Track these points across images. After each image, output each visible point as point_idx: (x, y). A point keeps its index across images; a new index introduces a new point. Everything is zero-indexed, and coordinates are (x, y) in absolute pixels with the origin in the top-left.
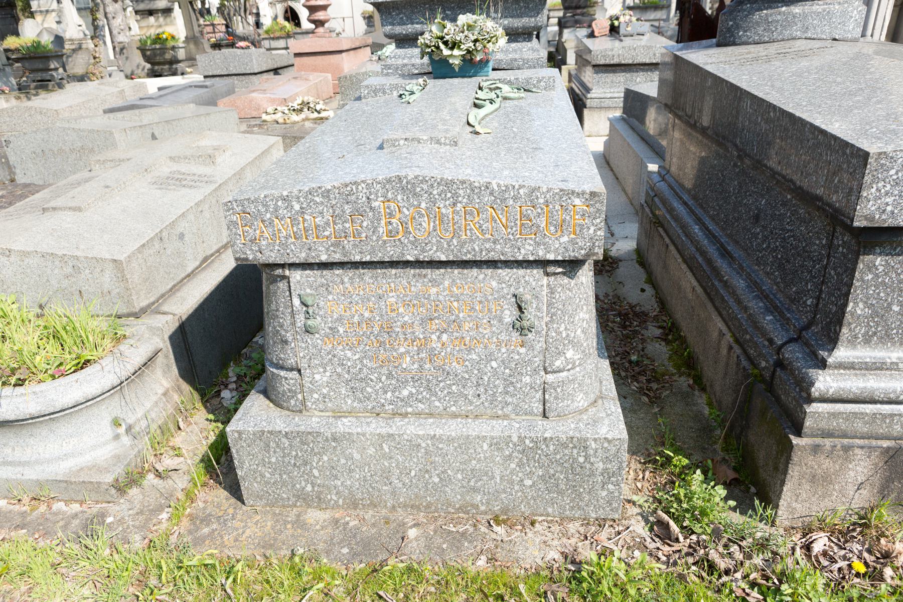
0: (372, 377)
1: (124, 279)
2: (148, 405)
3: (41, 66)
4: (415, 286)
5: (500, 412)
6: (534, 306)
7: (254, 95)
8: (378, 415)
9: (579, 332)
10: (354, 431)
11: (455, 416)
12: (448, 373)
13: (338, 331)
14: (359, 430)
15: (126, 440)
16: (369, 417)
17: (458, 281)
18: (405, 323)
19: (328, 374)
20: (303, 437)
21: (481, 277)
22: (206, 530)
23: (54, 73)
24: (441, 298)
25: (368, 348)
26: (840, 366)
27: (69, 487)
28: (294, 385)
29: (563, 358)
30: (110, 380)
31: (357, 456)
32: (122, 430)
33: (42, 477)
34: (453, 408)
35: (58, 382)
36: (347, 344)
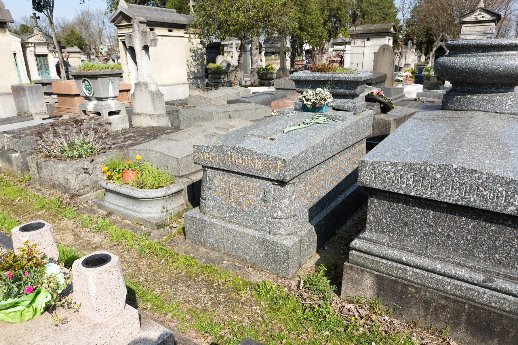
1: (178, 165)
2: (175, 206)
3: (218, 77)
7: (287, 101)
9: (284, 206)
10: (215, 223)
11: (244, 226)
15: (165, 214)
20: (203, 221)
22: (173, 244)
23: (222, 80)
26: (364, 238)
27: (145, 222)
30: (163, 194)
31: (215, 232)
32: (165, 210)
33: (141, 217)
35: (152, 190)
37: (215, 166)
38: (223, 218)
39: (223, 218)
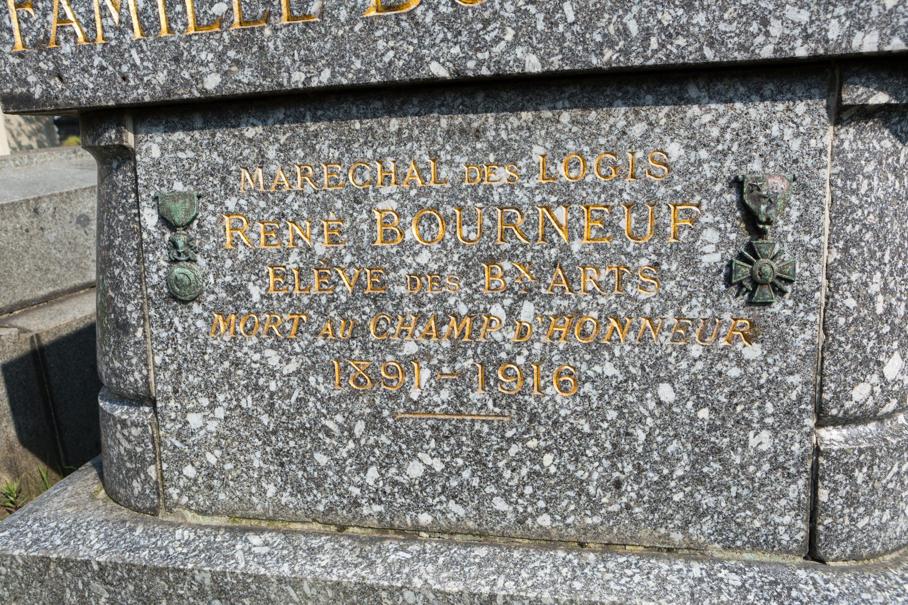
0: (330, 424)
4: (450, 163)
5: (677, 537)
6: (795, 214)
8: (342, 528)
11: (547, 542)
12: (533, 417)
13: (248, 295)
14: (285, 569)
16: (318, 534)
17: (571, 145)
18: (420, 272)
19: (220, 413)
21: (638, 130)
24: (521, 195)
25: (321, 342)
28: (140, 441)
29: (875, 379)
34: (545, 520)
36: (270, 332)
37: (212, 82)
38: (326, 518)
39: (326, 518)
